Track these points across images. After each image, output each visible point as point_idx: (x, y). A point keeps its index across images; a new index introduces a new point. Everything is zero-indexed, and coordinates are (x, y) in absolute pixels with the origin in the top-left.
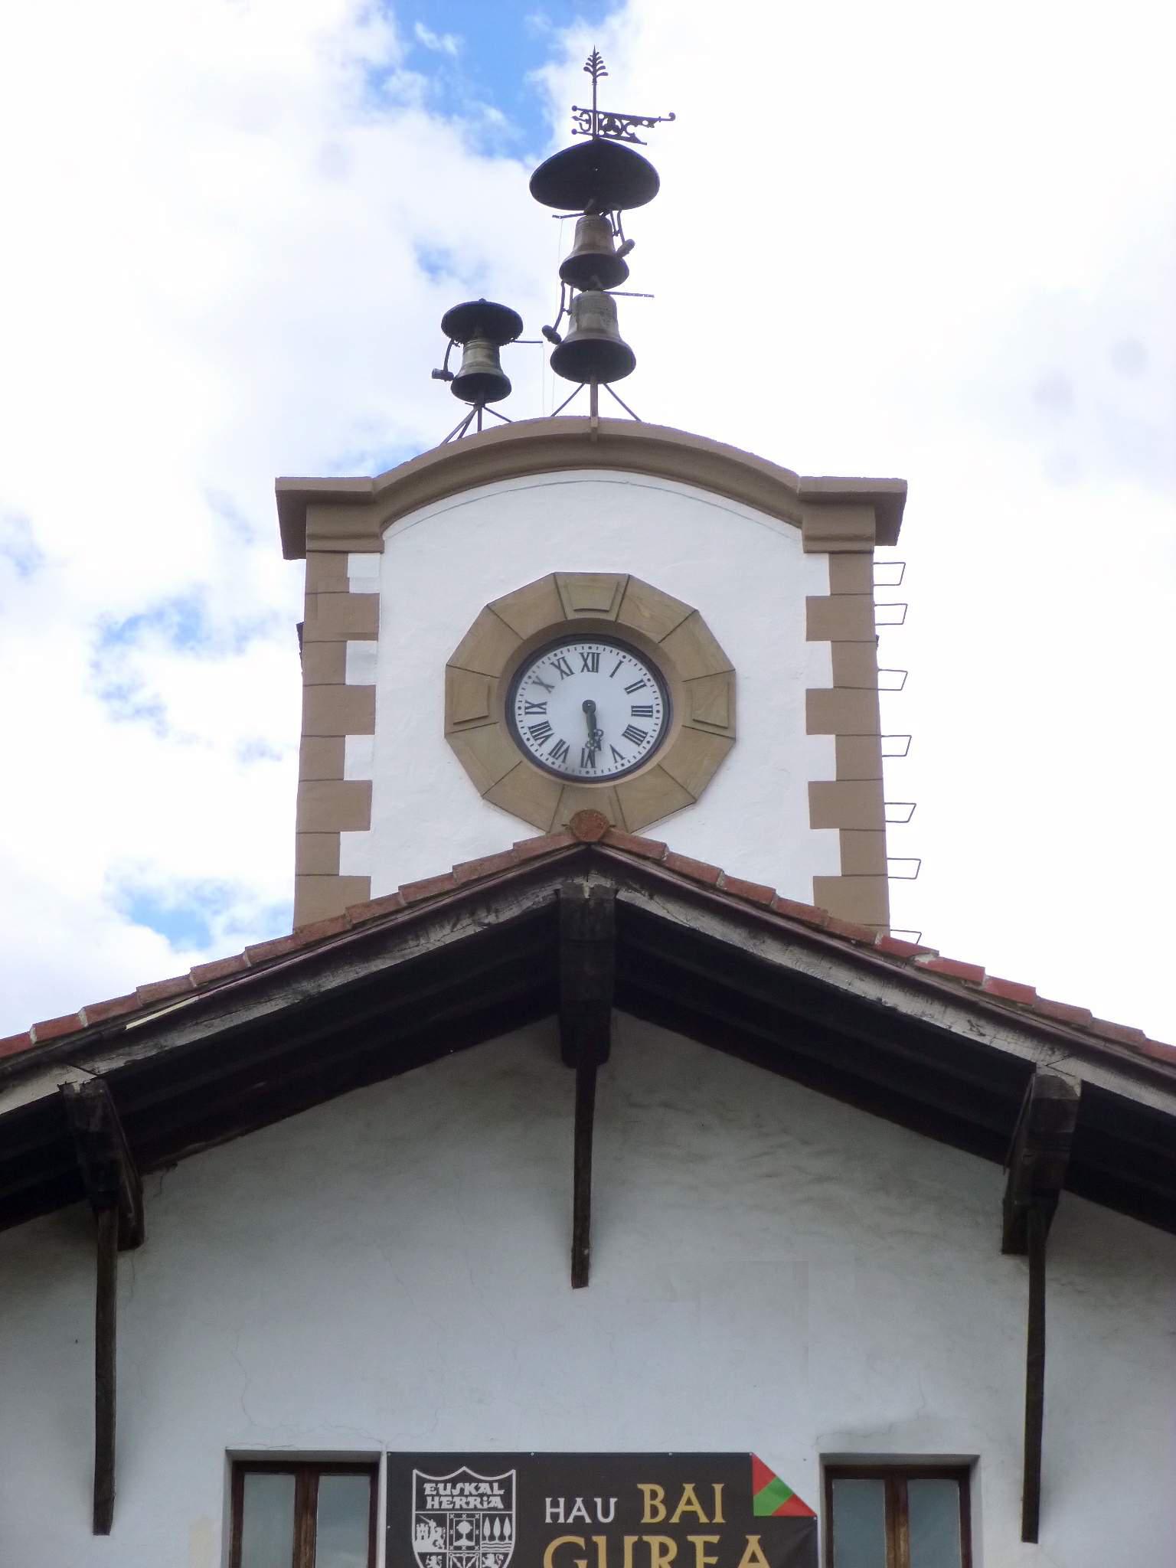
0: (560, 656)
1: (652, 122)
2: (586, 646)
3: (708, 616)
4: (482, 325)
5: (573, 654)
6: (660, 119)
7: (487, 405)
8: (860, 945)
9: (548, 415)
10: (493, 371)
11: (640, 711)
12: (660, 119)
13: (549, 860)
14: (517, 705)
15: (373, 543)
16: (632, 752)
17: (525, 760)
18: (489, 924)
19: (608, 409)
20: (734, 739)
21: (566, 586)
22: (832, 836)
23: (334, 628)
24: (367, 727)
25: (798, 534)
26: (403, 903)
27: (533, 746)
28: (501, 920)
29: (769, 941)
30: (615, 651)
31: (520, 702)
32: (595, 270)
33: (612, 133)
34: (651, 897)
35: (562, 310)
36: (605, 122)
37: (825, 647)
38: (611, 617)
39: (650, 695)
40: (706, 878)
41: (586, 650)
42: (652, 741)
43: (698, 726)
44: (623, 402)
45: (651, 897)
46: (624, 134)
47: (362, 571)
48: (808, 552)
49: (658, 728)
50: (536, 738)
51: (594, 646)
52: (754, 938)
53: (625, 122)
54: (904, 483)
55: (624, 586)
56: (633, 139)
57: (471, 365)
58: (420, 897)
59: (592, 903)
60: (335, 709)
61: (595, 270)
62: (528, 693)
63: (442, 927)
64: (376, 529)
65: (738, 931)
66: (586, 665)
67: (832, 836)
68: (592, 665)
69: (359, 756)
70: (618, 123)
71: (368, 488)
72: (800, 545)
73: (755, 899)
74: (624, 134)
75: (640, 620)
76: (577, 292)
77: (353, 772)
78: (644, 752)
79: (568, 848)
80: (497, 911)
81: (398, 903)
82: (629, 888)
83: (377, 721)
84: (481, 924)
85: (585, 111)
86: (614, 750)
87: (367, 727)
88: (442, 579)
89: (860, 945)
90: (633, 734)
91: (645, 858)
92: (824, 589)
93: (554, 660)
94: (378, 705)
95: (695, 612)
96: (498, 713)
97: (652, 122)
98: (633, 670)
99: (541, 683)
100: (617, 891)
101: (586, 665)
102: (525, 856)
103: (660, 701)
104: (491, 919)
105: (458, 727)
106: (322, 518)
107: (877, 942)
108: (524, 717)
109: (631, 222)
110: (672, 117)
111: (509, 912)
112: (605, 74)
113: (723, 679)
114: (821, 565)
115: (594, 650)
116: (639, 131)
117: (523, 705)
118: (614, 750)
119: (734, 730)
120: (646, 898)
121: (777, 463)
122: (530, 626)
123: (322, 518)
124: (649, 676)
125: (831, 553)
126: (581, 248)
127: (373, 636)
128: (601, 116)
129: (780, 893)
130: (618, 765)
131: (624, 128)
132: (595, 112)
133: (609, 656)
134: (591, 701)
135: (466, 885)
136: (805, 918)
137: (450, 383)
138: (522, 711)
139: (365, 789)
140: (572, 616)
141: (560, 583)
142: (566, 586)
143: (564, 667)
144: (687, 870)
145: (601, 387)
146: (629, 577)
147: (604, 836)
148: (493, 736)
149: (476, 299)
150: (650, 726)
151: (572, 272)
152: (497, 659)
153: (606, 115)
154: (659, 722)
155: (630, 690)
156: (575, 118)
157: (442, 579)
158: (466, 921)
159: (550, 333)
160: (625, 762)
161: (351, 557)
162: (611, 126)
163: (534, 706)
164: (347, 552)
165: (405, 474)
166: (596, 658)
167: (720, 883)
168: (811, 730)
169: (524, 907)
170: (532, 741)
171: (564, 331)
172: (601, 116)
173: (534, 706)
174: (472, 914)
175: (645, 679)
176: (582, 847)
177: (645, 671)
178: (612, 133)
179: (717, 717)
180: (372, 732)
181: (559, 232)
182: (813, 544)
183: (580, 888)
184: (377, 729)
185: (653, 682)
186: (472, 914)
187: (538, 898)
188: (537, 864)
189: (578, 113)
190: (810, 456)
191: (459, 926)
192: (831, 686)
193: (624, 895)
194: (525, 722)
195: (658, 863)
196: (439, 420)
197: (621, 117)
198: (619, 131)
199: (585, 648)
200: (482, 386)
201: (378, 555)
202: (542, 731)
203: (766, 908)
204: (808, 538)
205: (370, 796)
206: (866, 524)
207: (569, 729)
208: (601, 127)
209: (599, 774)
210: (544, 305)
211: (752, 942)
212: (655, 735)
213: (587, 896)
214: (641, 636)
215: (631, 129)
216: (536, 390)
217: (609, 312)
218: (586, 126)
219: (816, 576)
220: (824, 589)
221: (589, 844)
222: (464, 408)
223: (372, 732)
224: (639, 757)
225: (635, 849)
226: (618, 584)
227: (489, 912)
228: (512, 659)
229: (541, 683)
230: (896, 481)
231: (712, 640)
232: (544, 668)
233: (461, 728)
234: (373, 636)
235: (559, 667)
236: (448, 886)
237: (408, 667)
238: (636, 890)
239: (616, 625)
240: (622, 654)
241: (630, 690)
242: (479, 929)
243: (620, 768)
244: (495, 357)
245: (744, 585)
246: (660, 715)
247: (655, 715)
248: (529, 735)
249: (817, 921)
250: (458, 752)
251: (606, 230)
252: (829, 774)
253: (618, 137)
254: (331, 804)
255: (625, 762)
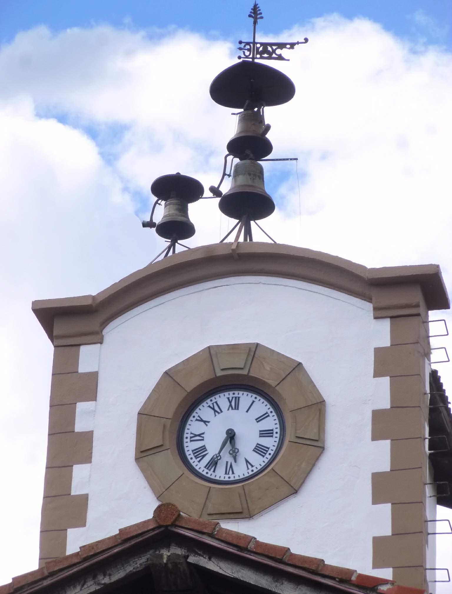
0: (214, 401)
1: (292, 45)
2: (231, 393)
3: (307, 365)
4: (177, 190)
5: (222, 399)
6: (298, 43)
7: (179, 241)
8: (342, 581)
9: (218, 241)
10: (180, 219)
11: (266, 433)
12: (298, 43)
13: (140, 539)
14: (185, 435)
15: (96, 337)
16: (258, 461)
17: (187, 473)
18: (105, 584)
19: (258, 236)
20: (323, 448)
21: (216, 354)
22: (386, 509)
23: (71, 389)
24: (87, 459)
25: (369, 306)
26: (46, 573)
27: (194, 462)
28: (112, 581)
29: (286, 583)
30: (250, 394)
31: (187, 434)
32: (251, 146)
33: (266, 55)
34: (210, 559)
35: (224, 174)
36: (261, 49)
37: (386, 381)
38: (245, 372)
39: (272, 423)
40: (242, 544)
41: (231, 395)
42: (272, 453)
43: (301, 441)
44: (269, 231)
45: (210, 559)
46: (274, 55)
47: (88, 358)
48: (376, 318)
49: (276, 444)
50: (196, 457)
51: (236, 392)
52: (277, 581)
53: (274, 47)
54: (438, 266)
55: (254, 351)
56: (280, 58)
57: (170, 215)
58: (56, 569)
59: (170, 566)
60: (67, 447)
61: (251, 146)
62: (193, 427)
63: (75, 587)
64: (96, 328)
65: (266, 577)
66: (231, 405)
67: (386, 509)
68: (235, 405)
69: (81, 478)
70: (270, 49)
71: (89, 302)
72: (372, 315)
73: (273, 555)
74: (274, 55)
75: (263, 372)
76: (237, 160)
77: (76, 490)
78: (266, 461)
79: (153, 530)
80: (110, 575)
81: (43, 573)
82: (196, 554)
83: (94, 454)
84: (99, 584)
85: (248, 43)
86: (247, 461)
87: (87, 459)
88: (137, 359)
89: (342, 581)
90: (260, 450)
91: (203, 533)
92: (386, 342)
93: (210, 403)
94: (94, 444)
95: (299, 364)
96: (170, 442)
97: (292, 45)
98: (262, 406)
99: (201, 420)
100: (188, 556)
101: (231, 405)
102: (125, 537)
103: (278, 426)
104: (106, 580)
105: (144, 453)
106: (70, 322)
107: (354, 578)
108: (189, 444)
109: (271, 114)
110: (306, 40)
111: (118, 574)
112: (262, 18)
113: (317, 407)
114: (386, 325)
115: (236, 395)
116: (284, 52)
117: (189, 436)
118: (247, 461)
119: (324, 442)
120: (206, 560)
121: (354, 261)
122: (192, 383)
123: (70, 322)
124: (271, 409)
125: (391, 317)
126: (240, 133)
127: (94, 398)
128: (258, 45)
129: (293, 551)
130: (250, 471)
131: (274, 51)
132: (254, 43)
133: (246, 398)
134: (236, 427)
135: (85, 559)
136: (306, 566)
137: (154, 230)
138: (188, 440)
139: (377, 499)
140: (219, 373)
141: (213, 352)
142: (216, 354)
143: (216, 408)
144: (230, 539)
145: (252, 223)
146: (257, 344)
147: (176, 520)
148: (167, 459)
149: (174, 172)
150: (271, 443)
151: (236, 147)
152: (169, 408)
153: (262, 44)
154: (277, 440)
155: (258, 420)
156: (240, 49)
157: (137, 359)
158: (90, 583)
159: (215, 191)
160: (254, 468)
161: (83, 349)
162: (265, 51)
163: (196, 436)
164: (80, 345)
165: (113, 292)
166: (237, 399)
167: (251, 546)
168: (375, 438)
169: (128, 571)
170: (194, 459)
171: (226, 188)
172: (258, 45)
173: (196, 436)
174: (94, 577)
175: (269, 411)
176: (162, 529)
177: (269, 406)
178: (266, 55)
179: (311, 434)
180: (90, 462)
181: (228, 122)
182: (379, 313)
183: (161, 556)
184: (93, 459)
185: (274, 413)
186: (94, 577)
187: (137, 564)
188: (133, 542)
189: (242, 46)
190: (375, 254)
191: (85, 586)
192: (388, 406)
193: (192, 559)
194: (190, 446)
195: (211, 535)
196: (154, 249)
197: (271, 45)
198: (270, 54)
199: (230, 394)
200: (176, 229)
201: (99, 345)
202: (200, 452)
203: (281, 561)
204: (375, 309)
205: (87, 504)
206: (416, 296)
207: (213, 442)
208: (258, 53)
209: (237, 478)
210: (214, 172)
211: (274, 585)
212: (274, 449)
213: (165, 561)
214: (264, 383)
215: (278, 52)
216: (210, 225)
217: (259, 173)
218: (247, 53)
219: (381, 333)
220: (386, 342)
221: (167, 526)
222: (164, 243)
223: (90, 462)
224: (263, 464)
225: (196, 528)
226: (250, 350)
227: (105, 576)
228: (180, 406)
229: (201, 420)
230: (431, 265)
231: (311, 382)
232: (204, 411)
233: (145, 454)
234: (94, 398)
235: (213, 409)
236: (76, 560)
237: (113, 420)
238: (200, 555)
239: (247, 377)
240: (254, 396)
241: (258, 420)
242: (98, 588)
243: (251, 473)
244: (184, 211)
245: (337, 350)
246: (278, 435)
247: (275, 435)
248: (192, 456)
249: (313, 567)
250: (143, 470)
251: (259, 119)
252: (386, 467)
253: (270, 58)
254: (62, 506)
255: (254, 468)
